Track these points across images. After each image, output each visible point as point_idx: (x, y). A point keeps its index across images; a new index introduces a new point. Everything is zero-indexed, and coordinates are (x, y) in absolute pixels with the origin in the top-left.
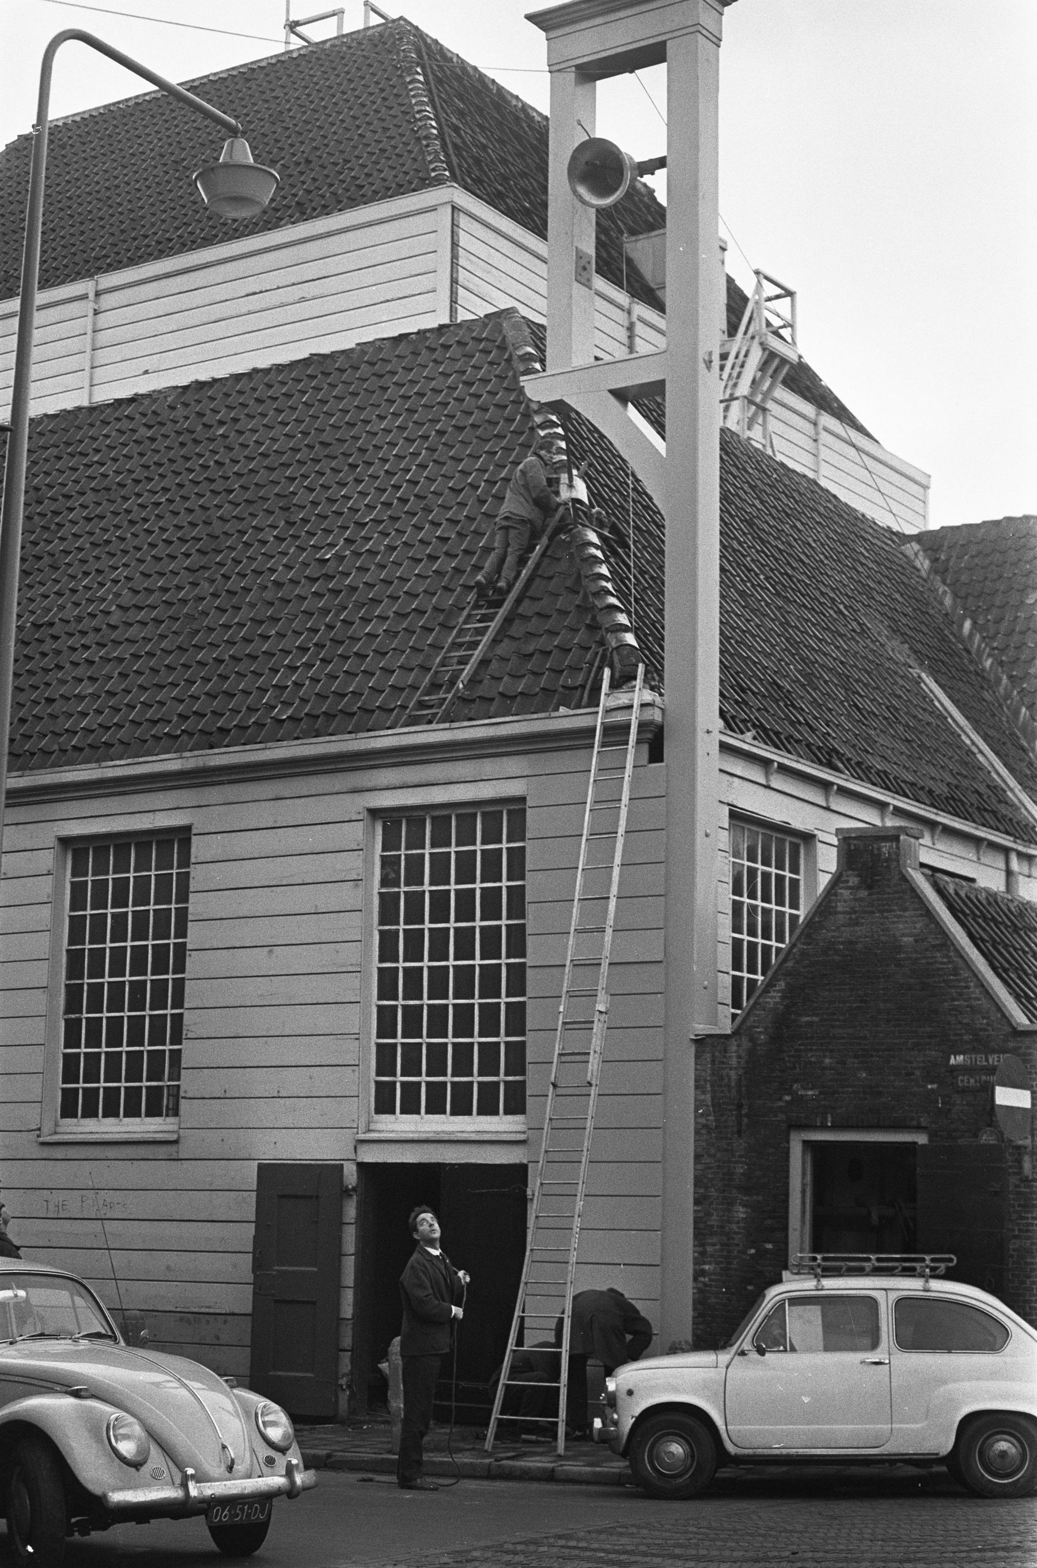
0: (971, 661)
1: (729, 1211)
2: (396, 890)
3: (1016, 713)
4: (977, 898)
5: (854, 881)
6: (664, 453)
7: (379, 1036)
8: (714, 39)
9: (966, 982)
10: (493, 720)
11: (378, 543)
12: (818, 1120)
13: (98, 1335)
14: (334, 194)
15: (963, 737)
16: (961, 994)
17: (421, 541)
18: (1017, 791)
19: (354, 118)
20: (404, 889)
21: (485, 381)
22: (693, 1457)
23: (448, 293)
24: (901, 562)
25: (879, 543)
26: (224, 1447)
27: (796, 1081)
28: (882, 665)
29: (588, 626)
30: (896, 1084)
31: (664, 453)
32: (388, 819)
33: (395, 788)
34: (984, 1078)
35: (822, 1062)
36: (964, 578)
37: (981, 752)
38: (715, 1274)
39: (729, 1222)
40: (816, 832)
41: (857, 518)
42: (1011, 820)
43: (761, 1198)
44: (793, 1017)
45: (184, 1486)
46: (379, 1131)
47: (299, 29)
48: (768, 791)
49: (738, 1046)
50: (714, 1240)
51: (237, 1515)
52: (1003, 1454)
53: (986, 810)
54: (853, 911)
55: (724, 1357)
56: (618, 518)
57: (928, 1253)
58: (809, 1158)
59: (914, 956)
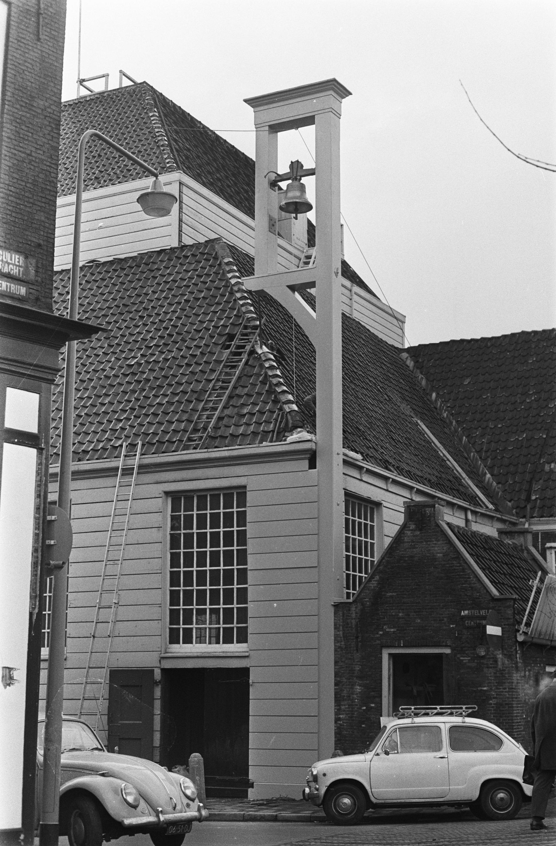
0: (438, 414)
1: (352, 688)
2: (179, 532)
3: (461, 440)
4: (459, 532)
5: (413, 527)
6: (315, 317)
7: (170, 605)
10: (230, 448)
11: (159, 356)
12: (396, 643)
13: (97, 749)
14: (115, 173)
15: (439, 452)
16: (466, 581)
17: (181, 356)
18: (466, 479)
19: (123, 134)
20: (183, 531)
21: (208, 275)
22: (355, 804)
23: (178, 226)
24: (401, 363)
25: (391, 354)
26: (171, 798)
27: (385, 624)
28: (400, 417)
29: (273, 401)
30: (435, 625)
31: (315, 317)
32: (175, 497)
33: (178, 481)
34: (478, 621)
35: (398, 615)
36: (432, 371)
37: (448, 460)
38: (346, 720)
39: (353, 694)
40: (383, 502)
41: (379, 341)
42: (465, 494)
43: (368, 682)
44: (383, 593)
45: (158, 816)
46: (171, 653)
47: (84, 83)
49: (356, 608)
50: (346, 702)
51: (179, 830)
52: (502, 799)
53: (454, 489)
55: (369, 756)
56: (280, 346)
57: (465, 705)
58: (391, 662)
59: (443, 563)
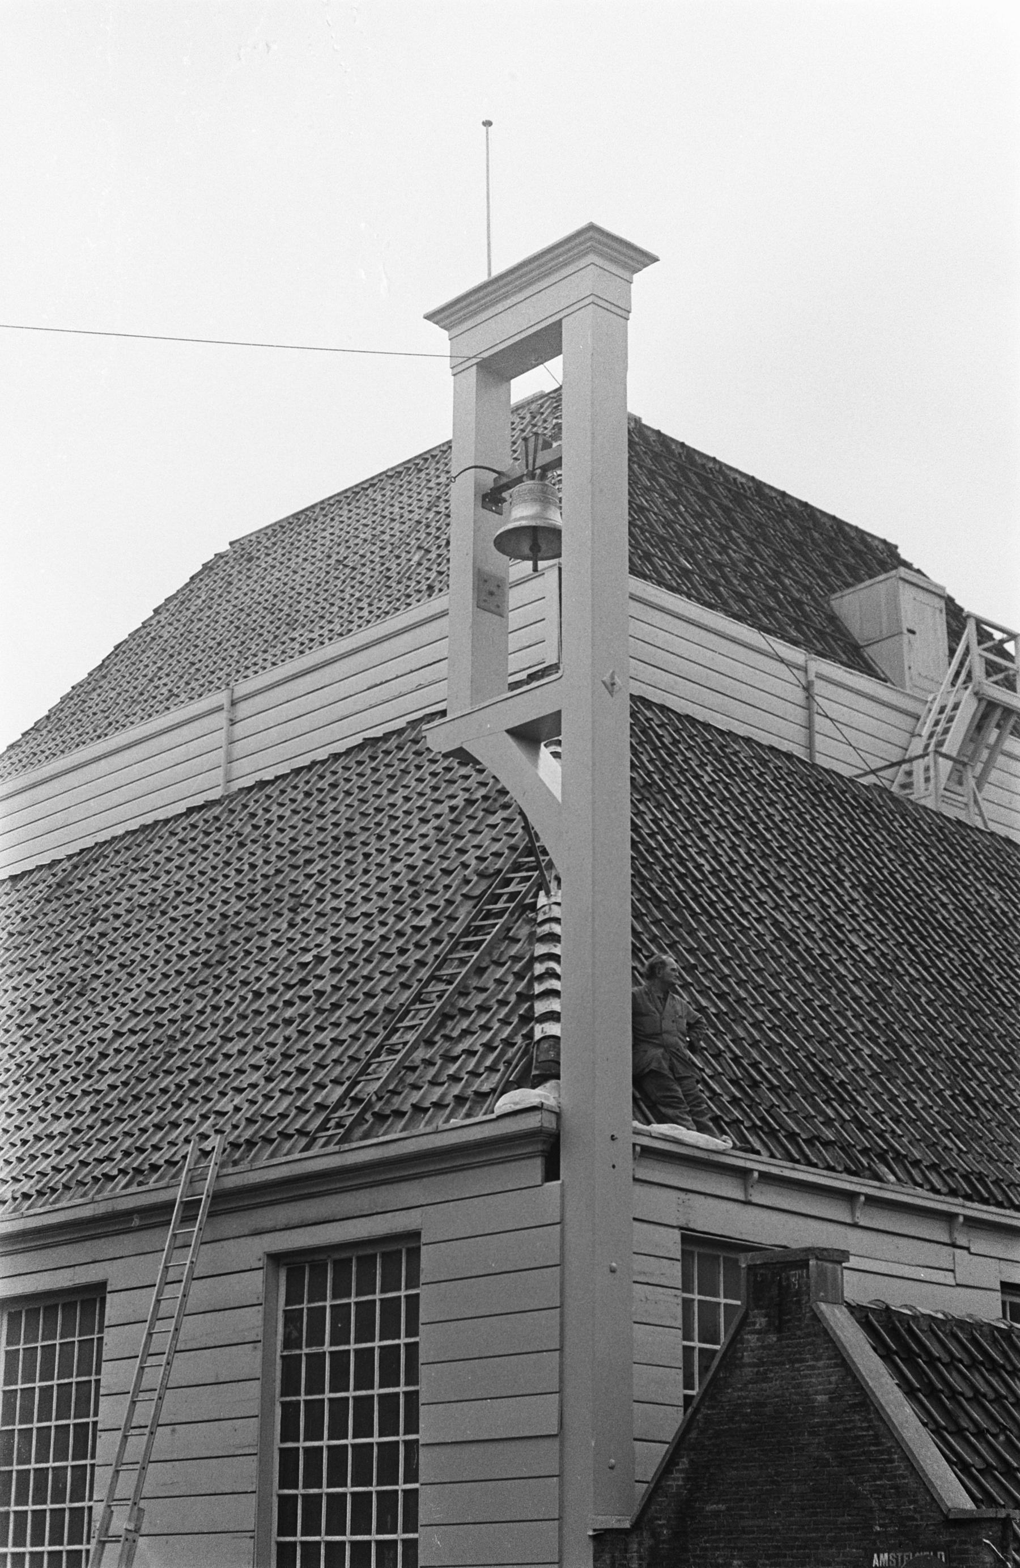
5: (761, 1322)
8: (619, 312)
9: (890, 1453)
32: (294, 1267)
44: (697, 1505)
48: (750, 1208)
49: (640, 1544)
54: (761, 1363)
